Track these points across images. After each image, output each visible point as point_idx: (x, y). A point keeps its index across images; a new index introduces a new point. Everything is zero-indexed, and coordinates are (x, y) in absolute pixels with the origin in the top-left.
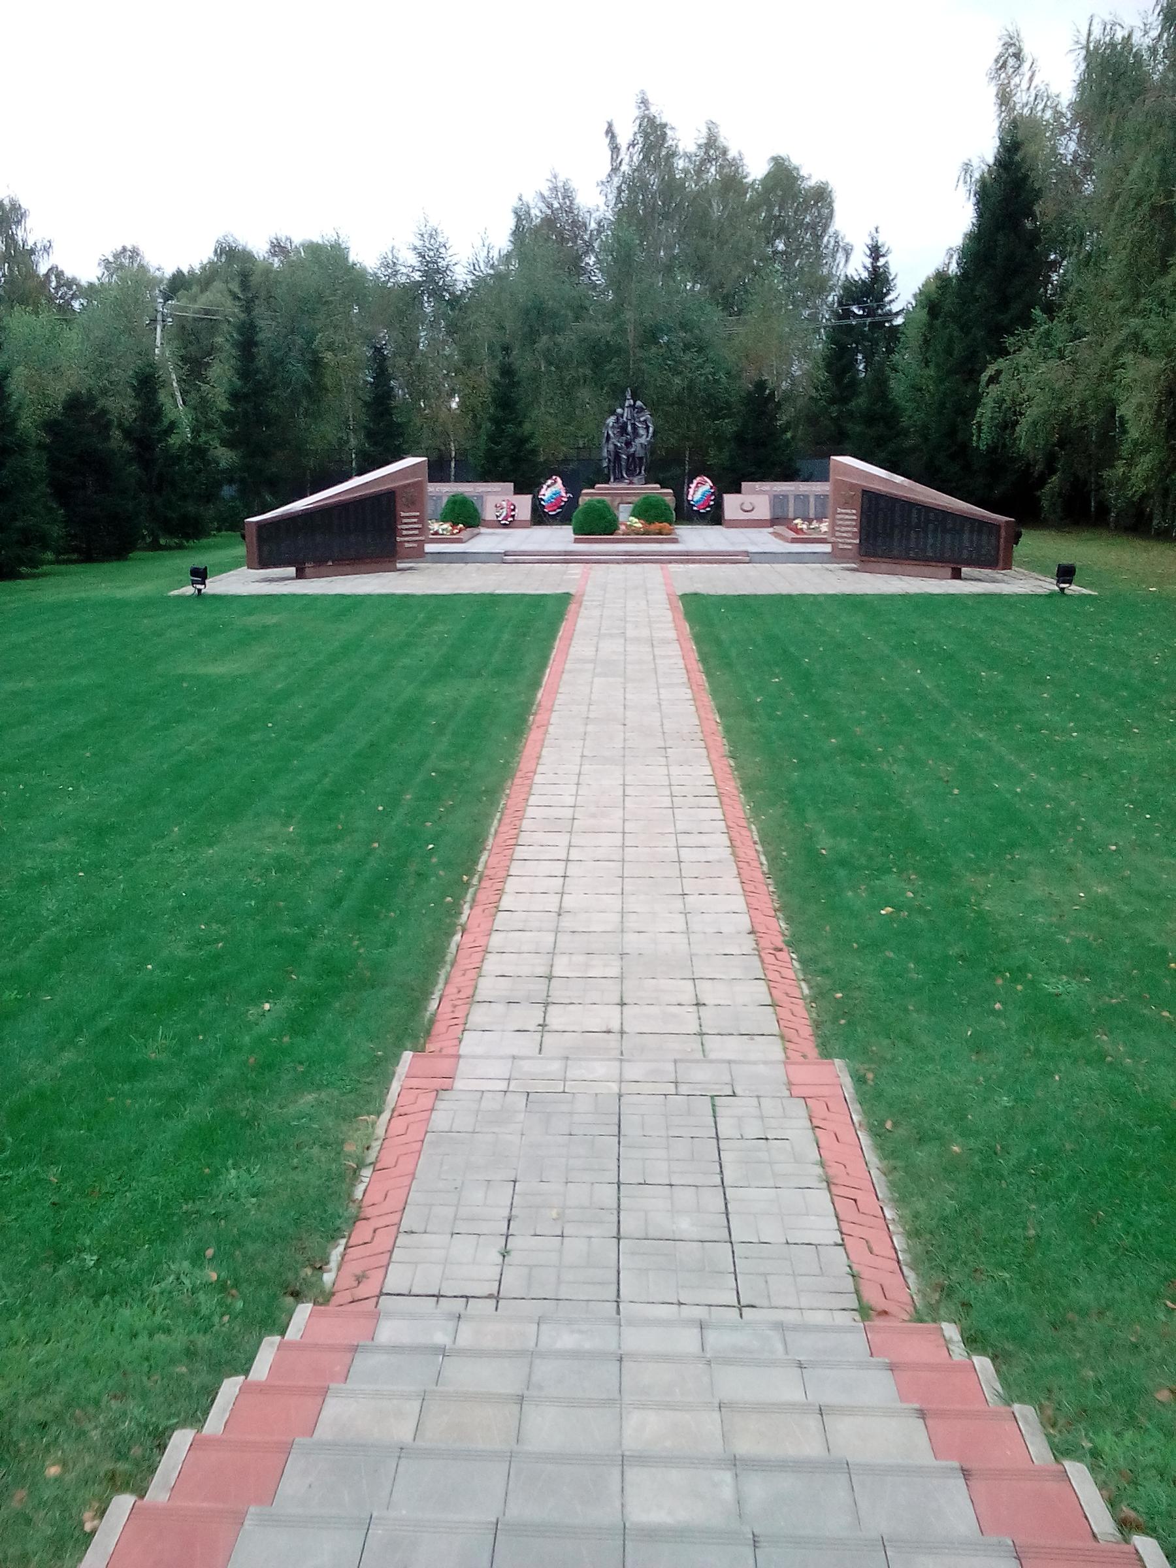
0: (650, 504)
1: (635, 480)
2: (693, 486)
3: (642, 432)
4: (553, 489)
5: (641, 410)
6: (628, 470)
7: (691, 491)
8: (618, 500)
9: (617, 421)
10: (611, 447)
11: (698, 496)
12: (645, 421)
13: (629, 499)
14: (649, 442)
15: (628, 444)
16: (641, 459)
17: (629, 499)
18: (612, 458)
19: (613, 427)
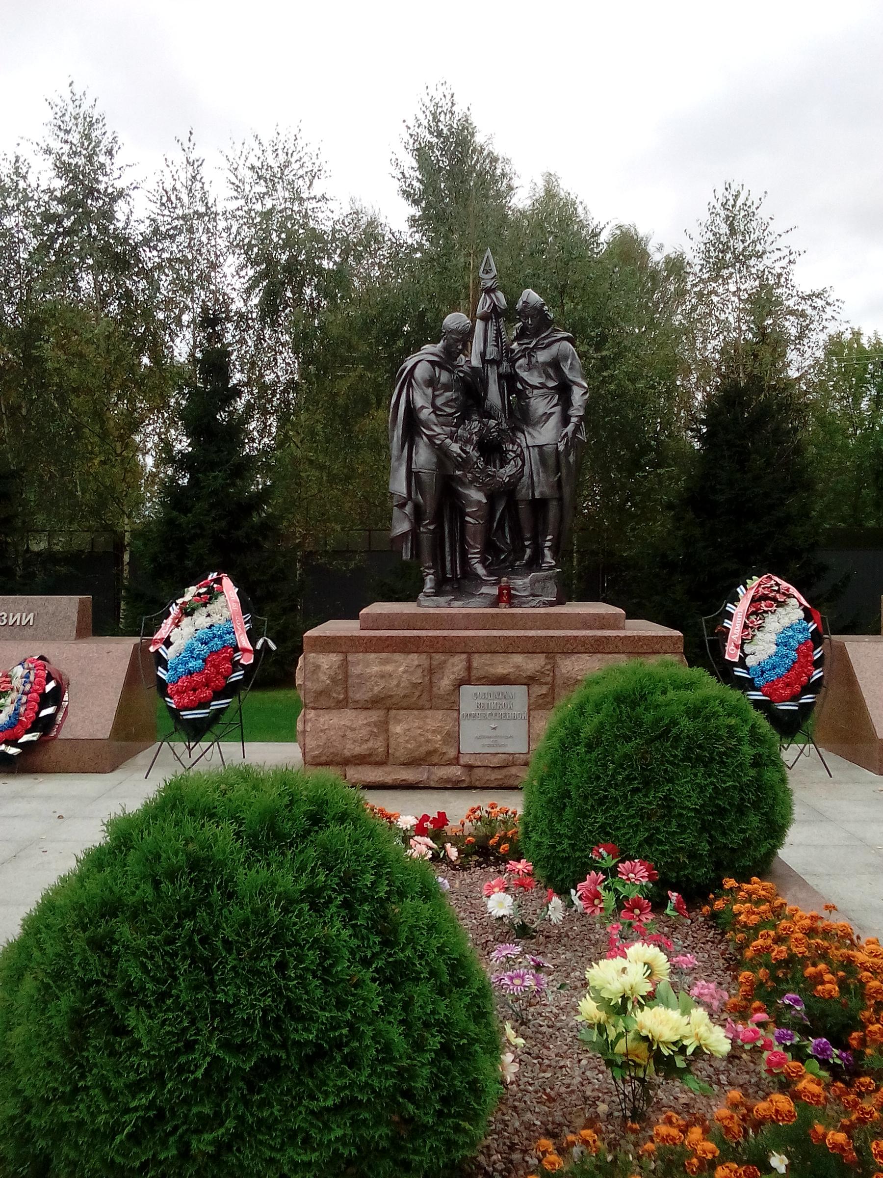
0: (664, 733)
1: (521, 583)
2: (739, 610)
3: (540, 405)
4: (201, 620)
5: (537, 324)
6: (490, 548)
7: (735, 628)
8: (456, 665)
9: (447, 360)
10: (423, 456)
11: (763, 649)
12: (555, 364)
13: (503, 666)
14: (573, 443)
15: (491, 449)
16: (539, 506)
17: (503, 666)
18: (428, 502)
19: (432, 382)
